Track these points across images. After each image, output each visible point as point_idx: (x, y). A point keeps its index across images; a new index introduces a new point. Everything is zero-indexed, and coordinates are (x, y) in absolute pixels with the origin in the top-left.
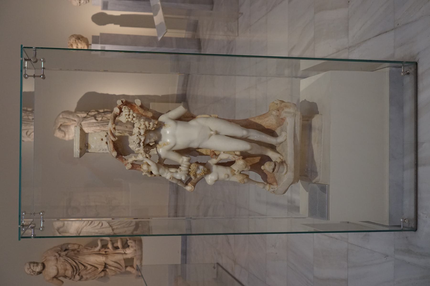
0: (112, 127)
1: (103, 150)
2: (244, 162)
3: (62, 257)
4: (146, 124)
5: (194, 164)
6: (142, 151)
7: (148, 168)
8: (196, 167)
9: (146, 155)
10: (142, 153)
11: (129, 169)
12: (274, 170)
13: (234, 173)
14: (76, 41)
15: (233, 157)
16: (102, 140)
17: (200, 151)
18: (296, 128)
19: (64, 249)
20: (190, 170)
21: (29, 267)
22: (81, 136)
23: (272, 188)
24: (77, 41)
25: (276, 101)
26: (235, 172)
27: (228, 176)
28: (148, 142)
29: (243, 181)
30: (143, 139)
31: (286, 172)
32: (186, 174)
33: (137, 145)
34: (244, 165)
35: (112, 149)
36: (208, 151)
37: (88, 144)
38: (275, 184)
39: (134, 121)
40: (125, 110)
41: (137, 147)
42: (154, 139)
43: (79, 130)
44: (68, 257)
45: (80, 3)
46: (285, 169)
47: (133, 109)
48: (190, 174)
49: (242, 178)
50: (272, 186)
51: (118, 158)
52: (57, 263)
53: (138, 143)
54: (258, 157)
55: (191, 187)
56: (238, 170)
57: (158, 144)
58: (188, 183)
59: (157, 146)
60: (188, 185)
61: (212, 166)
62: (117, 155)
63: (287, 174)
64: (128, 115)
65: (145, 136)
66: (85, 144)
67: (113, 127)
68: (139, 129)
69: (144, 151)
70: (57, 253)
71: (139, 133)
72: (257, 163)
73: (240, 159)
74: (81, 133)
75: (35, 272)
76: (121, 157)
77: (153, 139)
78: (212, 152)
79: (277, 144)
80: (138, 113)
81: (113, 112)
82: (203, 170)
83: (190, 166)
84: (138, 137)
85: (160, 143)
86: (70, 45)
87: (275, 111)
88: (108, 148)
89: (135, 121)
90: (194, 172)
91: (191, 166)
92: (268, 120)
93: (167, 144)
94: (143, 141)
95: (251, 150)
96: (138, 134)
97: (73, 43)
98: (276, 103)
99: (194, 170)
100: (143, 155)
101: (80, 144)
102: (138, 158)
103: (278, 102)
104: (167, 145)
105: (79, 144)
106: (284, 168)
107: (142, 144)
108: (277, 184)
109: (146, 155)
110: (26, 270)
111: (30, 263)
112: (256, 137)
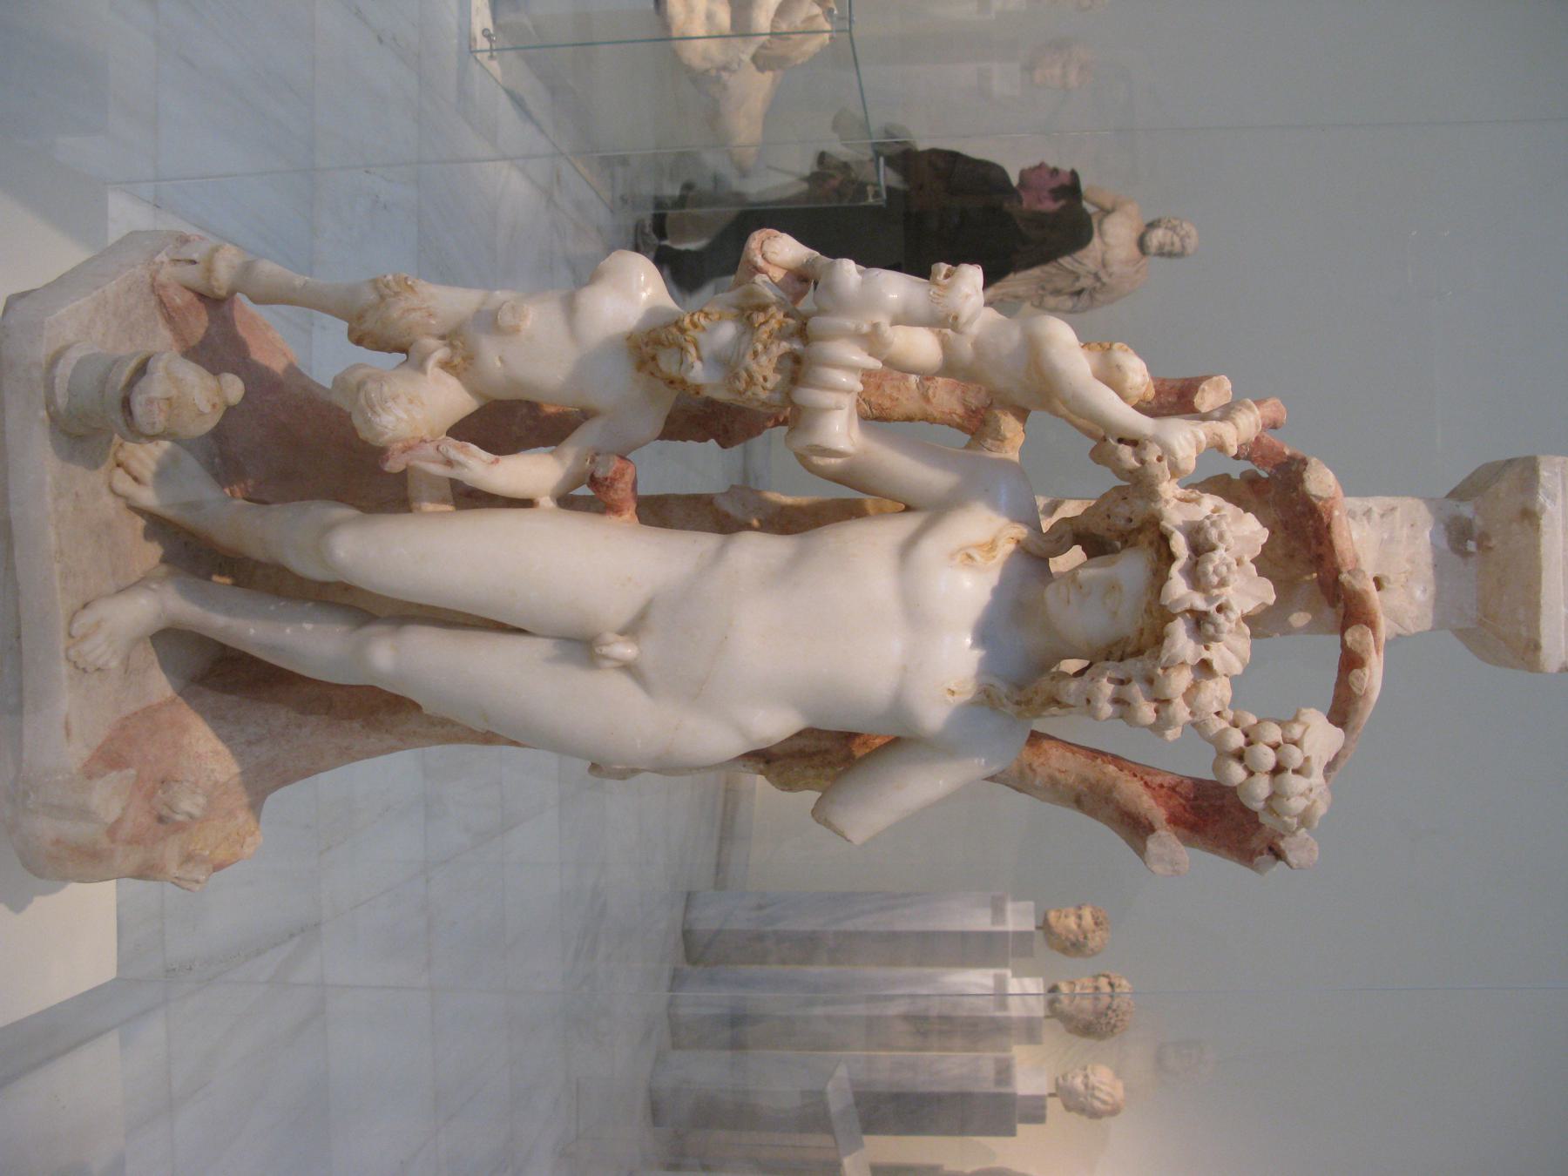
1: (1368, 513)
2: (368, 421)
3: (1089, 272)
8: (744, 375)
9: (1142, 462)
13: (452, 346)
14: (1085, 938)
15: (459, 463)
16: (1378, 583)
19: (1085, 296)
21: (1187, 241)
23: (194, 262)
24: (1081, 939)
25: (197, 882)
26: (441, 353)
29: (387, 291)
30: (1178, 586)
35: (1336, 513)
38: (179, 299)
43: (1544, 642)
44: (1073, 272)
45: (1086, 1077)
47: (1183, 802)
50: (192, 275)
51: (1287, 452)
52: (1104, 253)
53: (1213, 548)
55: (770, 256)
64: (1290, 772)
70: (1104, 284)
73: (400, 445)
75: (1166, 228)
80: (1146, 777)
84: (1218, 597)
86: (1101, 924)
87: (179, 817)
90: (764, 328)
93: (969, 557)
94: (1175, 570)
95: (331, 527)
96: (1221, 618)
97: (1094, 931)
99: (760, 347)
100: (1160, 459)
101: (1535, 547)
102: (1202, 436)
105: (1543, 550)
107: (1179, 545)
108: (156, 289)
110: (1194, 232)
111: (1181, 254)
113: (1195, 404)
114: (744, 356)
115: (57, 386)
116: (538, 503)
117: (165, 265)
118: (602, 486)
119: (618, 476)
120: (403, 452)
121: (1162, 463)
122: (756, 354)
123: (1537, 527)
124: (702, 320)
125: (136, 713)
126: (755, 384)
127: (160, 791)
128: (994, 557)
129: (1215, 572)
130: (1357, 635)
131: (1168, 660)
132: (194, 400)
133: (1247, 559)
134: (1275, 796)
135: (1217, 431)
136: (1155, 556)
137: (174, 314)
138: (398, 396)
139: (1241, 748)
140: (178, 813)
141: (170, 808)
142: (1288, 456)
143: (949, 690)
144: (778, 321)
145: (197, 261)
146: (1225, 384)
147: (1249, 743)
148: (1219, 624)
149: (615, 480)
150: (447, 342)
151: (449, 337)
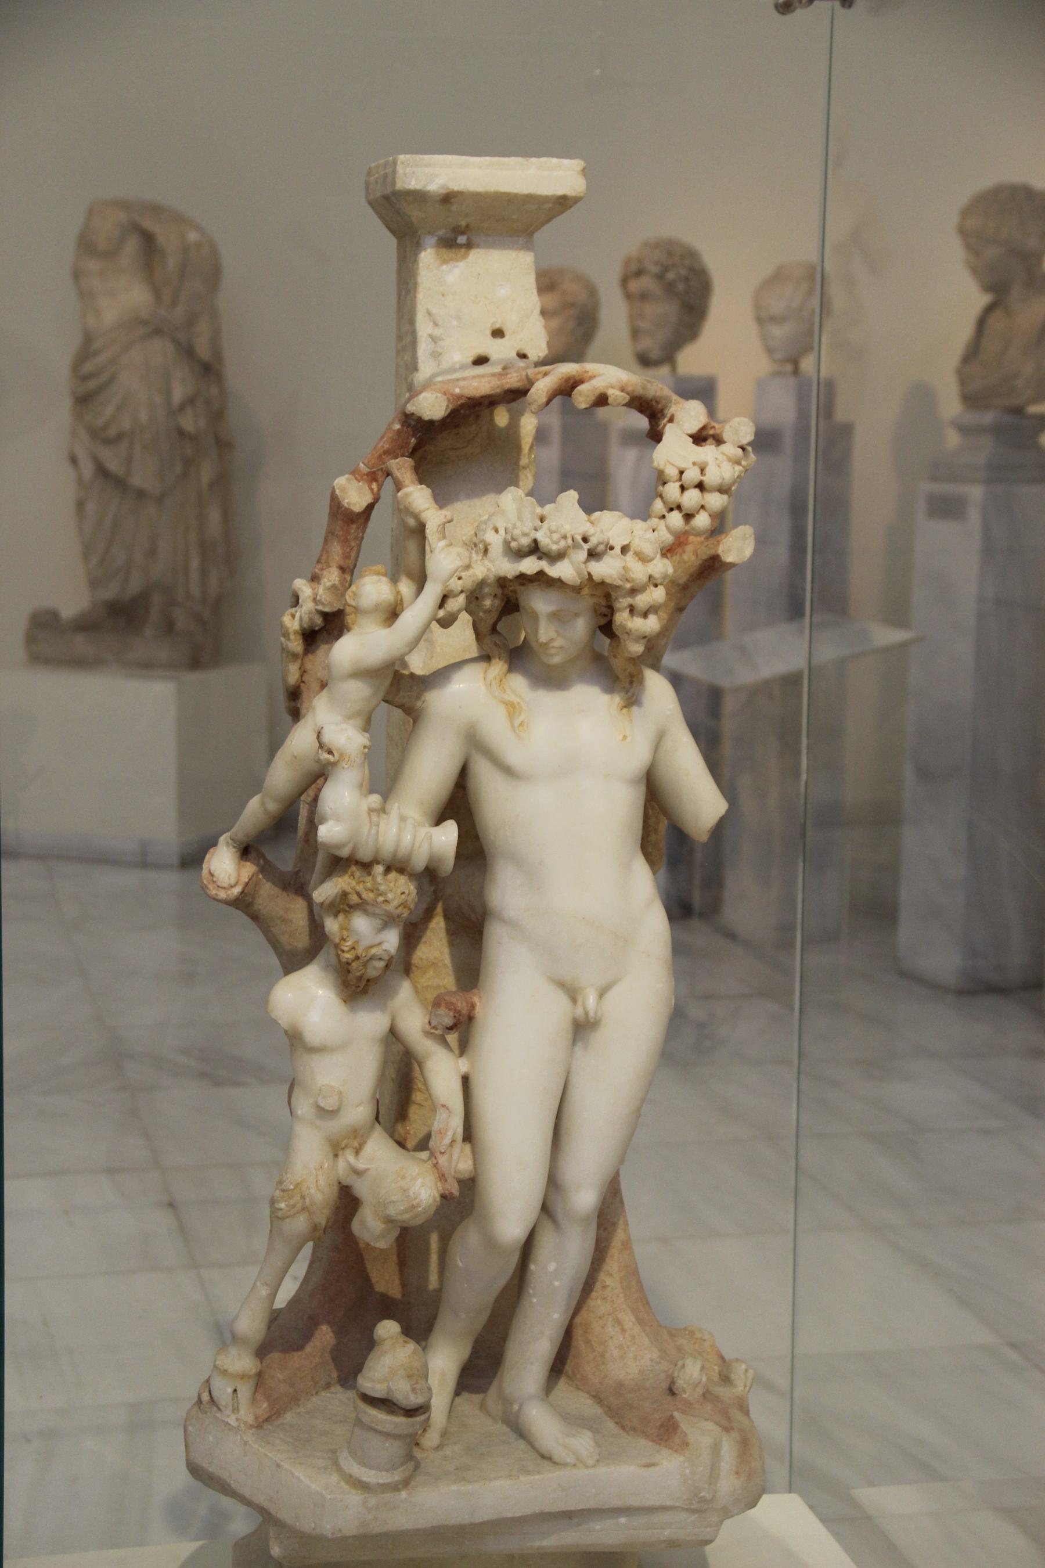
0: (607, 387)
1: (434, 339)
4: (648, 591)
5: (410, 899)
6: (482, 569)
7: (377, 608)
8: (399, 911)
9: (462, 592)
10: (471, 571)
11: (337, 492)
12: (385, 1404)
16: (498, 333)
17: (433, 925)
18: (623, 1520)
20: (379, 869)
22: (529, 198)
23: (235, 1390)
25: (746, 1371)
27: (324, 1113)
28: (540, 603)
29: (299, 1206)
30: (563, 571)
31: (362, 1486)
32: (354, 849)
33: (525, 535)
34: (406, 1211)
35: (457, 391)
36: (431, 973)
37: (469, 246)
39: (664, 517)
40: (730, 460)
41: (514, 539)
42: (556, 644)
43: (560, 192)
46: (384, 1478)
48: (352, 875)
49: (319, 1197)
50: (245, 1391)
51: (398, 426)
53: (535, 541)
54: (397, 1282)
55: (233, 881)
56: (366, 1171)
57: (510, 670)
58: (258, 865)
59: (495, 661)
60: (243, 863)
61: (383, 1007)
62: (420, 419)
63: (346, 1487)
64: (703, 478)
65: (577, 589)
66: (467, 226)
67: (610, 392)
68: (625, 550)
69: (482, 584)
71: (601, 548)
72: (367, 1279)
73: (439, 1184)
74: (544, 199)
76: (407, 444)
77: (553, 635)
78: (467, 1003)
79: (506, 1401)
81: (675, 397)
82: (373, 951)
83: (401, 871)
85: (518, 682)
87: (704, 1379)
88: (452, 370)
89: (662, 522)
90: (364, 895)
91: (403, 880)
92: (623, 1331)
93: (521, 724)
94: (555, 571)
98: (733, 1376)
99: (381, 899)
103: (741, 1388)
104: (513, 726)
106: (387, 1471)
107: (530, 565)
109: (462, 592)
112: (552, 1267)
113: (360, 511)
114: (386, 911)
115: (386, 1481)
116: (465, 1073)
117: (239, 1417)
118: (459, 1019)
119: (453, 1007)
120: (446, 1181)
121: (463, 577)
122: (386, 901)
123: (459, 193)
124: (349, 943)
125: (616, 1423)
126: (406, 901)
127: (684, 1396)
128: (518, 703)
129: (557, 543)
130: (581, 399)
131: (621, 580)
132: (406, 1357)
133: (539, 510)
134: (722, 490)
135: (435, 529)
136: (534, 584)
137: (275, 1409)
138: (401, 1188)
139: (683, 516)
140: (701, 1380)
141: (697, 1384)
142: (403, 426)
143: (623, 740)
144: (357, 884)
145: (234, 1388)
146: (341, 482)
147: (679, 507)
148: (598, 542)
149: (455, 1010)
150: (340, 1153)
151: (336, 1148)
